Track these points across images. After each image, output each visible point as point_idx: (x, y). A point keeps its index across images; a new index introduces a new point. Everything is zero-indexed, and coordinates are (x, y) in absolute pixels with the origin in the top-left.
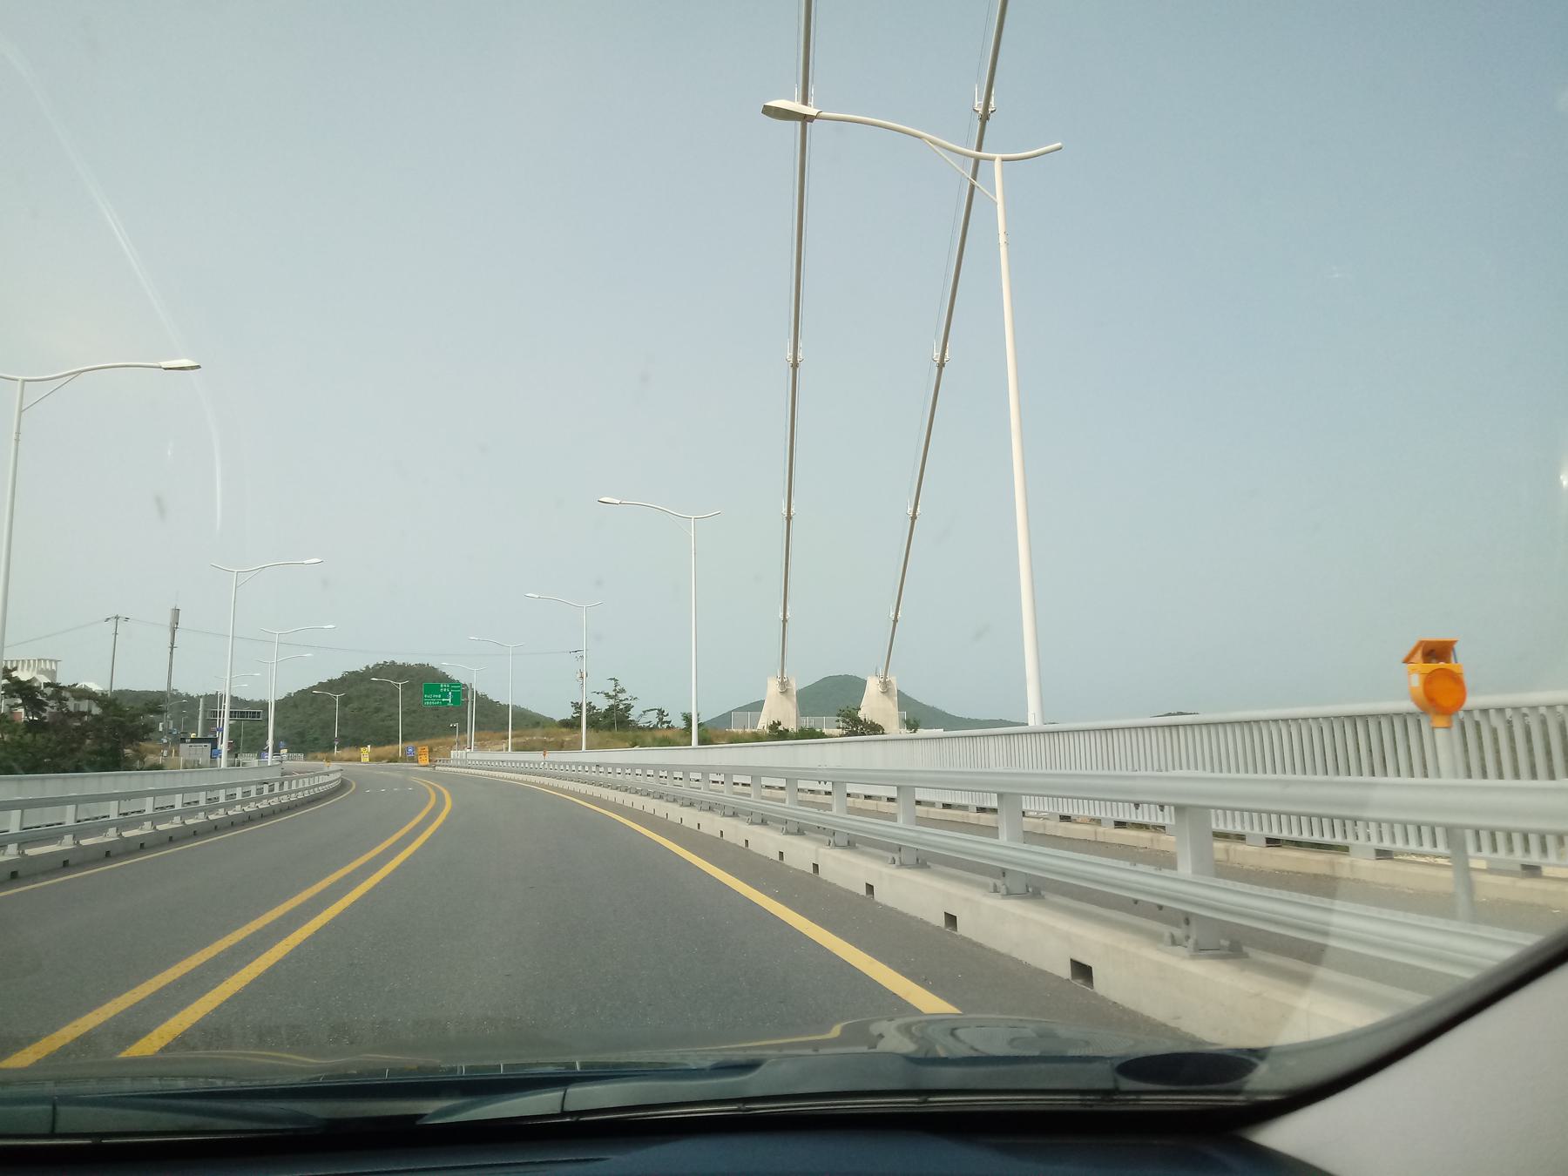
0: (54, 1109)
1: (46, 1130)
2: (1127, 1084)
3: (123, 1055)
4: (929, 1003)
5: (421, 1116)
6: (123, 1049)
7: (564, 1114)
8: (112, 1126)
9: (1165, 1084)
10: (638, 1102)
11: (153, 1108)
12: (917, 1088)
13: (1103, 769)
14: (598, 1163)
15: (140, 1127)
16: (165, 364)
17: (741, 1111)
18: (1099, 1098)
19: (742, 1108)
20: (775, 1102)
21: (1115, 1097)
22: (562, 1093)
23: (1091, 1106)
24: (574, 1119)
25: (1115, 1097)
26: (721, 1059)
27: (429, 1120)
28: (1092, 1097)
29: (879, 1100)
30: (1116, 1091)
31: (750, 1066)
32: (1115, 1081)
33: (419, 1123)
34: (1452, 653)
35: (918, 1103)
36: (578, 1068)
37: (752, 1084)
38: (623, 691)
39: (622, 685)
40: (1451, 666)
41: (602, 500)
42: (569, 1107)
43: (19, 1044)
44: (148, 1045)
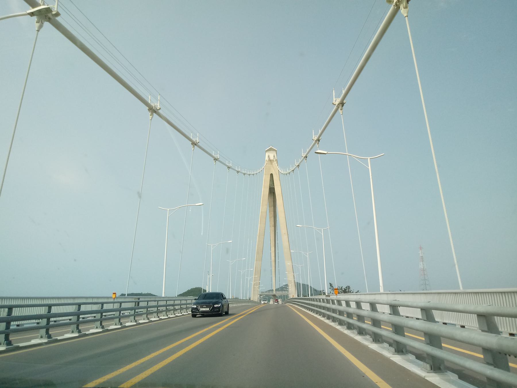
16: (196, 205)
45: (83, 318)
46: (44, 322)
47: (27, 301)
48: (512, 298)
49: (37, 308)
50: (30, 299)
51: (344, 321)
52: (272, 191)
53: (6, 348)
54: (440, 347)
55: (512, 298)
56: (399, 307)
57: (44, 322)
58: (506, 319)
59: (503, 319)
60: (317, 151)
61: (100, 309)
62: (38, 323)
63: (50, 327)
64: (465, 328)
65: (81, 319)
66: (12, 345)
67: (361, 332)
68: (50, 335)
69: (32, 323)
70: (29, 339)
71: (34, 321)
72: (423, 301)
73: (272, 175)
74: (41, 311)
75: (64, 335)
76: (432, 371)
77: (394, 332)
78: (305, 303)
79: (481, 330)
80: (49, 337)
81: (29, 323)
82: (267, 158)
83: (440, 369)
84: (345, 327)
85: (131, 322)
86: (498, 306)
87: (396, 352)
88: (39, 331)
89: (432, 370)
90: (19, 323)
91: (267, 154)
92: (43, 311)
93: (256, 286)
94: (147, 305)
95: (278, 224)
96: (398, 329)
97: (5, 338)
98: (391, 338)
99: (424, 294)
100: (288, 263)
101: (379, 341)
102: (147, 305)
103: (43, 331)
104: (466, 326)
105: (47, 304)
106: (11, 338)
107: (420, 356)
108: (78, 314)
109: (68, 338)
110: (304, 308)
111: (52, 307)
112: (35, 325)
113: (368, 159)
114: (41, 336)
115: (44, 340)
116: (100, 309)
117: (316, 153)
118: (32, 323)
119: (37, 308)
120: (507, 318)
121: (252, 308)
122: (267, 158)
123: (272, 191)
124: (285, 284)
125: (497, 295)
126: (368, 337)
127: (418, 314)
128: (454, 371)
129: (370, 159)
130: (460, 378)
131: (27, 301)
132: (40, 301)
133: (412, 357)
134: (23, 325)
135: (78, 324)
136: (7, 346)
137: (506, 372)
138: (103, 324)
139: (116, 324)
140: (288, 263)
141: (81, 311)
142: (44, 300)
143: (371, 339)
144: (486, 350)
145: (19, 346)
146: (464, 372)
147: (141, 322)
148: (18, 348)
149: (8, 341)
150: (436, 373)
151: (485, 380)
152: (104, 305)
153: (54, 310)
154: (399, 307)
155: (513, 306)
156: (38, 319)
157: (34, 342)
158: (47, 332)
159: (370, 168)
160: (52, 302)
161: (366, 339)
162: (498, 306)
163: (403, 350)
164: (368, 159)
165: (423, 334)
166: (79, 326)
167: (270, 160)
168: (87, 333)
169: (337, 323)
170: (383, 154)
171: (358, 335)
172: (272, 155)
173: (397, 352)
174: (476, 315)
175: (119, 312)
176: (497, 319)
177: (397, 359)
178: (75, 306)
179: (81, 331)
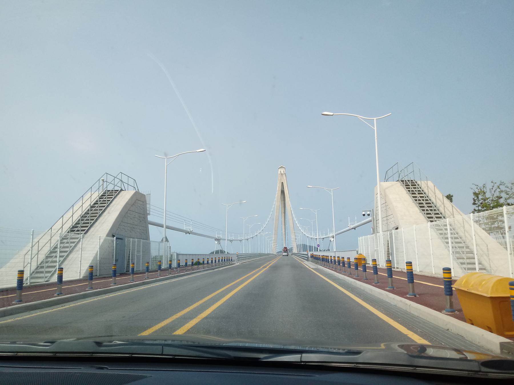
0: (163, 347)
1: (161, 353)
2: (484, 369)
3: (139, 335)
5: (260, 358)
7: (301, 362)
9: (500, 370)
11: (190, 349)
14: (312, 377)
15: (189, 355)
16: (198, 151)
17: (356, 366)
18: (474, 373)
19: (356, 365)
21: (480, 373)
22: (301, 355)
23: (471, 375)
24: (305, 363)
25: (480, 373)
27: (262, 360)
29: (386, 367)
30: (480, 371)
31: (358, 353)
32: (480, 368)
33: (259, 360)
34: (101, 243)
37: (359, 358)
41: (308, 186)
42: (303, 360)
43: (145, 329)
44: (180, 332)
52: (283, 192)
60: (323, 113)
73: (282, 183)
78: (303, 257)
79: (228, 260)
82: (279, 173)
91: (279, 170)
93: (272, 244)
95: (286, 213)
100: (293, 237)
110: (43, 373)
113: (374, 119)
117: (322, 114)
122: (279, 173)
123: (283, 192)
124: (291, 247)
129: (376, 119)
140: (293, 237)
159: (375, 129)
164: (374, 119)
167: (281, 174)
170: (391, 114)
172: (282, 170)
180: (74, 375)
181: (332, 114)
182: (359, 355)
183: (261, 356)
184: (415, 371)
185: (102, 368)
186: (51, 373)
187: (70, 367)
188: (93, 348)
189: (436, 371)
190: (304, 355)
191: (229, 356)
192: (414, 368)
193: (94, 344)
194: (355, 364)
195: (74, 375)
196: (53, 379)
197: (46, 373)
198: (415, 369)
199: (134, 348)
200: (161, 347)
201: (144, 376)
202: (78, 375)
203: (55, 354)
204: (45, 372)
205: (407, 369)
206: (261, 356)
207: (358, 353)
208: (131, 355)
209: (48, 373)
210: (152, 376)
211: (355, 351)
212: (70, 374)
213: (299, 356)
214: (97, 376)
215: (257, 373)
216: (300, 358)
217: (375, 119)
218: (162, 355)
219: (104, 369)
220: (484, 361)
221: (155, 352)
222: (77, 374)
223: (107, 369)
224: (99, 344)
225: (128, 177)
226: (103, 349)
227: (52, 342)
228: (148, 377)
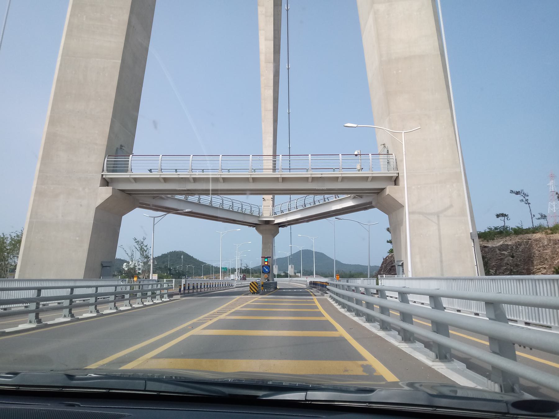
0: (146, 382)
1: (143, 389)
4: (390, 377)
5: (259, 396)
6: (120, 367)
7: (306, 400)
8: (163, 389)
10: (445, 406)
12: (432, 405)
13: (551, 295)
15: (177, 391)
19: (368, 405)
20: (358, 403)
24: (310, 402)
26: (10, 371)
28: (499, 415)
30: (508, 413)
31: (371, 391)
33: (258, 398)
35: (501, 416)
36: (310, 386)
37: (372, 397)
38: (248, 266)
39: (248, 265)
40: (28, 323)
42: (308, 398)
44: (129, 366)
45: (44, 305)
46: (66, 303)
47: (21, 283)
48: (503, 283)
49: (29, 292)
50: (3, 282)
51: (361, 312)
53: (37, 326)
54: (447, 335)
55: (503, 283)
56: (409, 294)
57: (33, 306)
58: (507, 306)
59: (507, 306)
60: (346, 125)
61: (35, 296)
62: (26, 307)
63: (40, 312)
64: (479, 315)
65: (41, 306)
66: (42, 323)
67: (370, 319)
68: (41, 319)
69: (20, 307)
70: (16, 325)
71: (11, 306)
72: (433, 286)
74: (46, 293)
75: (54, 320)
76: (438, 360)
77: (402, 320)
80: (72, 316)
81: (15, 307)
83: (446, 357)
84: (354, 313)
85: (126, 306)
86: (496, 291)
87: (437, 358)
88: (28, 315)
89: (437, 358)
90: (6, 307)
92: (32, 294)
94: (126, 289)
96: (406, 317)
97: (35, 317)
98: (489, 363)
99: (440, 280)
101: (387, 329)
102: (116, 290)
103: (32, 316)
104: (462, 310)
105: (37, 287)
106: (40, 317)
107: (428, 345)
108: (38, 300)
109: (110, 313)
111: (42, 290)
112: (23, 308)
113: (402, 133)
114: (64, 315)
115: (32, 325)
116: (35, 296)
117: (344, 126)
118: (20, 307)
119: (29, 292)
120: (543, 309)
121: (195, 320)
125: (514, 282)
126: (377, 324)
127: (426, 300)
128: (395, 329)
129: (405, 133)
130: (468, 367)
131: (21, 283)
132: (27, 284)
133: (462, 366)
134: (10, 308)
135: (96, 304)
136: (37, 324)
137: (516, 362)
138: (40, 317)
139: (111, 309)
141: (117, 292)
142: (37, 282)
143: (379, 327)
144: (493, 339)
145: (78, 318)
146: (471, 360)
147: (122, 308)
148: (47, 326)
149: (38, 320)
150: (442, 362)
151: (490, 368)
152: (74, 289)
153: (44, 293)
154: (409, 294)
155: (548, 295)
156: (26, 303)
157: (21, 327)
158: (37, 317)
160: (33, 285)
161: (375, 327)
162: (496, 291)
163: (515, 387)
164: (402, 133)
165: (487, 338)
166: (40, 314)
168: (80, 317)
169: (354, 313)
170: (420, 127)
171: (402, 343)
173: (438, 358)
174: (484, 302)
175: (95, 298)
176: (506, 307)
177: (404, 347)
178: (33, 290)
179: (42, 321)
180: (38, 412)
181: (355, 125)
182: (371, 394)
183: (260, 393)
184: (435, 412)
185: (73, 405)
186: (23, 410)
187: (36, 403)
188: (61, 381)
189: (462, 412)
190: (309, 393)
191: (223, 393)
192: (434, 409)
193: (65, 376)
194: (368, 404)
195: (38, 412)
196: (41, 416)
197: (6, 408)
198: (435, 410)
199: (112, 383)
200: (145, 381)
201: (122, 415)
202: (43, 413)
203: (18, 387)
204: (20, 409)
205: (407, 408)
206: (260, 393)
207: (371, 391)
208: (159, 393)
209: (8, 408)
210: (131, 415)
211: (368, 389)
212: (31, 411)
213: (303, 394)
214: (62, 414)
215: (250, 413)
216: (305, 396)
217: (403, 132)
218: (145, 391)
219: (75, 406)
220: (516, 401)
221: (138, 387)
222: (42, 411)
223: (79, 406)
224: (71, 377)
225: (154, 225)
226: (74, 383)
227: (16, 374)
228: (126, 416)
